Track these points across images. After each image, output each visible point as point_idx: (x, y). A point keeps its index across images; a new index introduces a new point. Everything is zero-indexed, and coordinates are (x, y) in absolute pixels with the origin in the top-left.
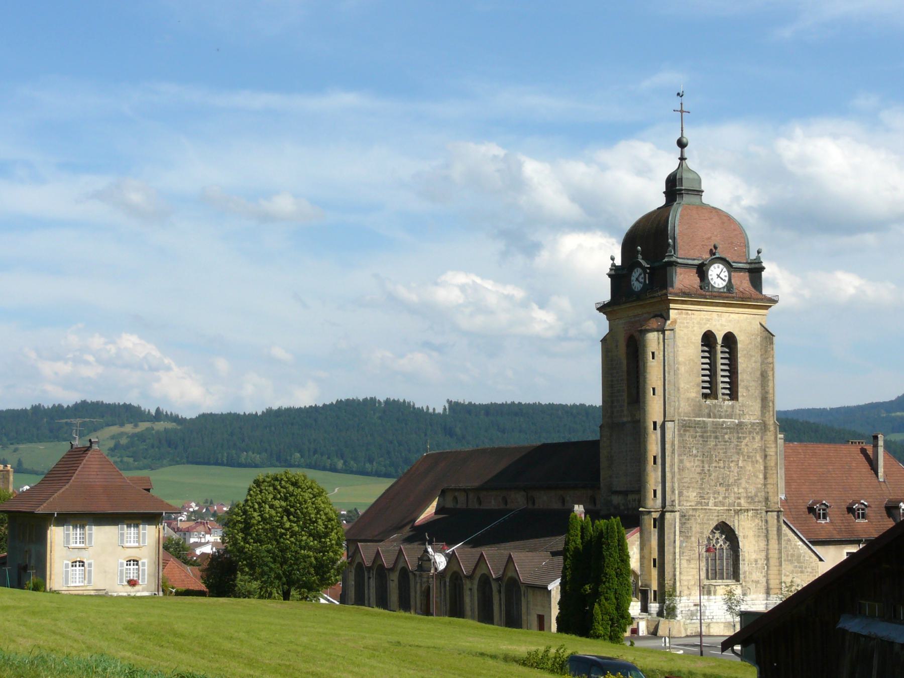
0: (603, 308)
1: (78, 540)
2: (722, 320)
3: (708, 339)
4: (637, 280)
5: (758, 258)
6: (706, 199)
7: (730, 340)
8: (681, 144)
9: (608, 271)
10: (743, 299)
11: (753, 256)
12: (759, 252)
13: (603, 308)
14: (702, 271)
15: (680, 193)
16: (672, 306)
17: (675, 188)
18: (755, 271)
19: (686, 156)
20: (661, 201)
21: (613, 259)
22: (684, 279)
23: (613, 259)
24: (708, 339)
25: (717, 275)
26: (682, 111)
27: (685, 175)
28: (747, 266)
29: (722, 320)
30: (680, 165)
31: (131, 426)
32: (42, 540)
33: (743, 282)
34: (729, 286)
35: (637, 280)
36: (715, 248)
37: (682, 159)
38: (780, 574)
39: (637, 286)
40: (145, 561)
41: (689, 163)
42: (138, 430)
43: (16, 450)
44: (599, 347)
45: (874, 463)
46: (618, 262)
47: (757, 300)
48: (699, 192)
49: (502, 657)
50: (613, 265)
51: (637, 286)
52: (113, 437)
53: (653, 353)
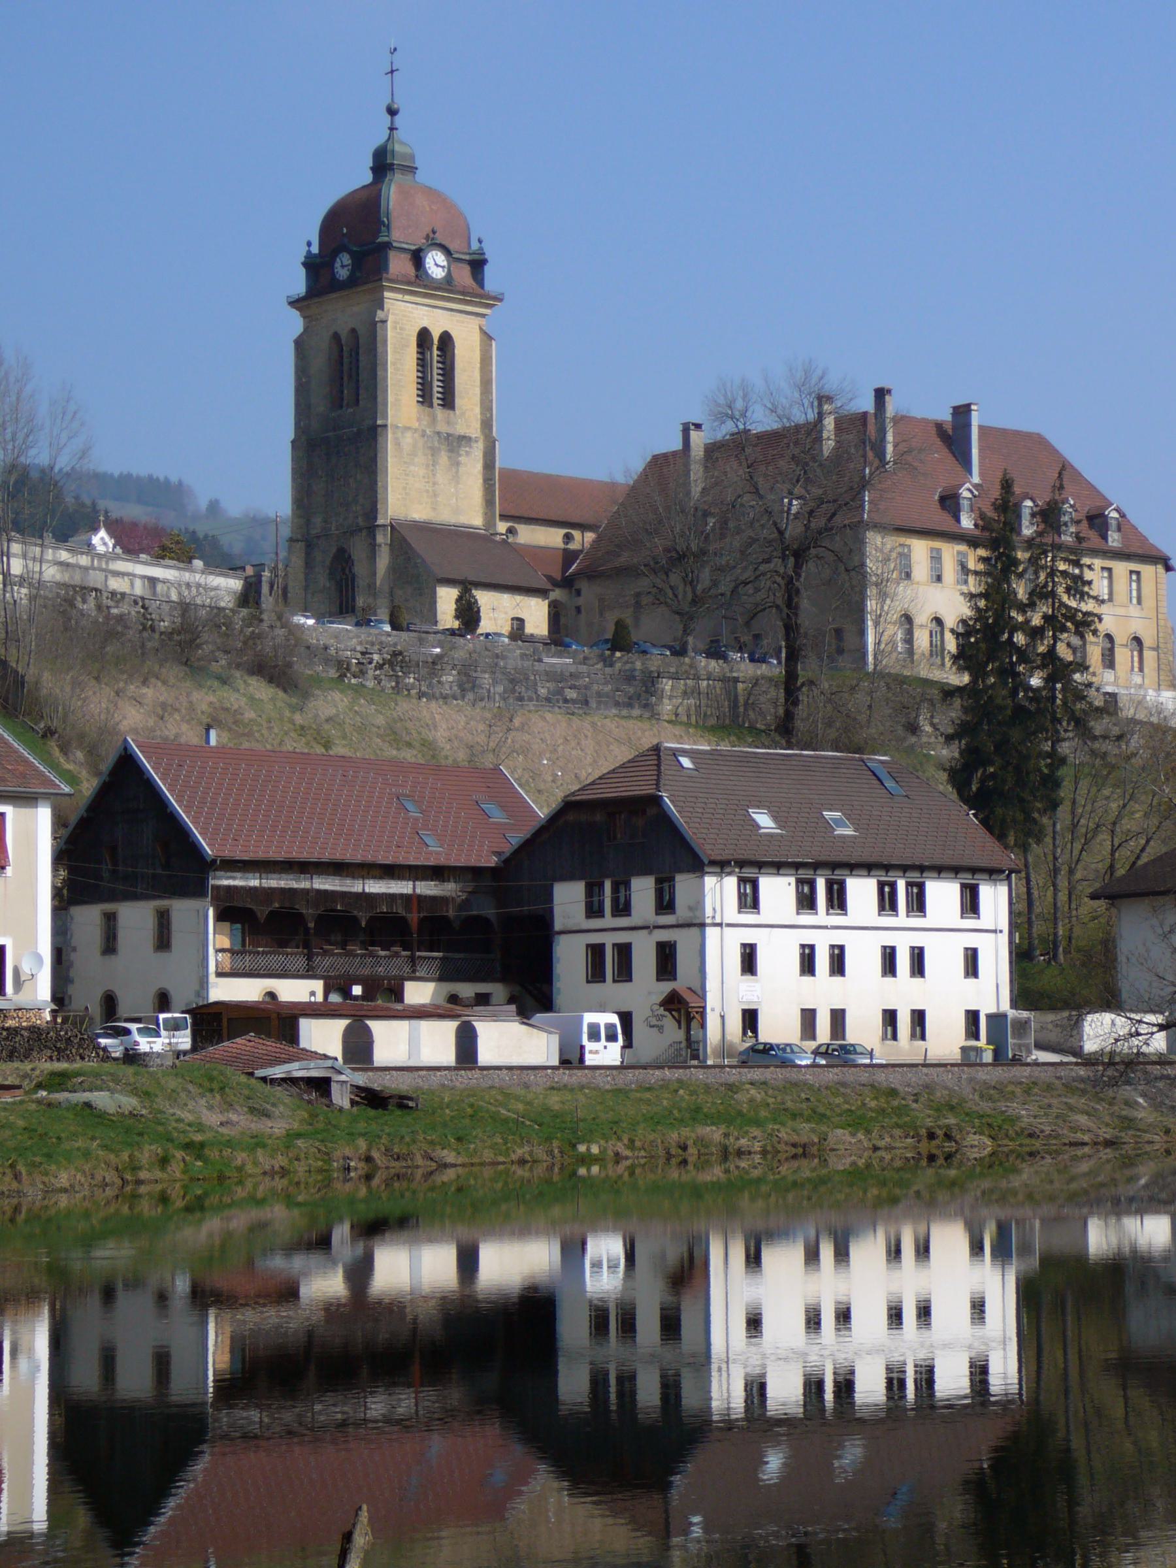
0: (295, 303)
2: (437, 319)
3: (424, 336)
4: (343, 267)
5: (481, 249)
6: (421, 177)
7: (446, 340)
8: (392, 112)
9: (303, 259)
10: (463, 293)
11: (475, 246)
13: (295, 303)
14: (417, 258)
15: (391, 167)
17: (383, 164)
18: (477, 265)
19: (397, 125)
20: (368, 178)
21: (309, 244)
22: (399, 264)
23: (309, 244)
24: (424, 336)
25: (436, 264)
27: (398, 148)
28: (467, 257)
32: (862, 542)
33: (464, 276)
34: (449, 279)
35: (343, 267)
36: (434, 232)
39: (342, 273)
44: (293, 345)
46: (315, 249)
47: (476, 296)
48: (412, 170)
49: (678, 985)
50: (309, 252)
51: (342, 273)
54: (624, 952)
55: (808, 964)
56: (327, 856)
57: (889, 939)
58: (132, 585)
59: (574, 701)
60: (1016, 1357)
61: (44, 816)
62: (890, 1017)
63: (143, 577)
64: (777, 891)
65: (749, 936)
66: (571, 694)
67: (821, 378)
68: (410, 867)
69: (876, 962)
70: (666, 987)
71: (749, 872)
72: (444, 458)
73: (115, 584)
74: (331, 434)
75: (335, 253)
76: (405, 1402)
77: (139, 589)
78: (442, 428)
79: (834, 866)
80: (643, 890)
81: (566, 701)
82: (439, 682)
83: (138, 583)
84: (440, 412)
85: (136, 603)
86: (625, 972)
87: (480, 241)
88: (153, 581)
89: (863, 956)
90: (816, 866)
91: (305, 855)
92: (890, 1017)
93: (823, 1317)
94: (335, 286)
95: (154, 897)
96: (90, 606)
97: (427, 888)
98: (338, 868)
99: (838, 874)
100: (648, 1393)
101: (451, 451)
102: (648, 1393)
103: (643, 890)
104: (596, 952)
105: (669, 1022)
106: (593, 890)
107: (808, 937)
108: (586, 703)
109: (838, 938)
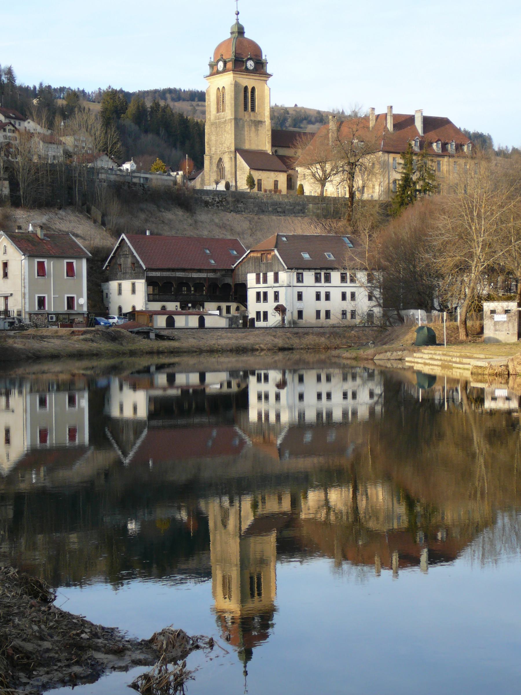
21: (211, 58)
23: (211, 58)
46: (212, 60)
54: (265, 294)
55: (318, 297)
56: (180, 267)
57: (344, 290)
58: (140, 180)
59: (280, 212)
60: (286, 397)
61: (84, 262)
62: (318, 313)
63: (143, 178)
64: (309, 277)
65: (300, 289)
66: (279, 210)
67: (360, 109)
68: (206, 270)
69: (340, 296)
70: (276, 304)
71: (300, 271)
72: (253, 129)
73: (135, 180)
74: (217, 121)
75: (218, 62)
76: (205, 420)
77: (142, 181)
78: (253, 118)
79: (327, 269)
80: (271, 276)
81: (278, 212)
82: (237, 207)
83: (142, 179)
84: (252, 113)
85: (141, 186)
86: (265, 299)
87: (266, 56)
88: (147, 179)
89: (336, 295)
90: (321, 269)
91: (173, 267)
92: (318, 313)
93: (326, 397)
94: (218, 72)
95: (131, 279)
96: (126, 188)
97: (211, 275)
98: (184, 270)
99: (328, 271)
100: (272, 418)
101: (255, 126)
102: (272, 418)
103: (271, 276)
104: (258, 294)
105: (277, 314)
106: (258, 276)
107: (318, 289)
108: (284, 212)
109: (328, 289)
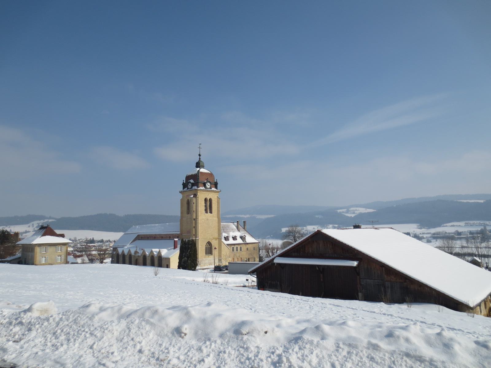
1: (189, 234)
5: (217, 181)
11: (216, 181)
12: (217, 180)
16: (198, 192)
21: (183, 181)
23: (183, 181)
24: (206, 200)
26: (200, 148)
29: (209, 195)
30: (199, 160)
31: (43, 220)
37: (200, 159)
38: (93, 352)
40: (63, 256)
41: (201, 160)
42: (44, 221)
43: (9, 227)
45: (440, 248)
50: (183, 182)
52: (38, 223)
53: (194, 203)
